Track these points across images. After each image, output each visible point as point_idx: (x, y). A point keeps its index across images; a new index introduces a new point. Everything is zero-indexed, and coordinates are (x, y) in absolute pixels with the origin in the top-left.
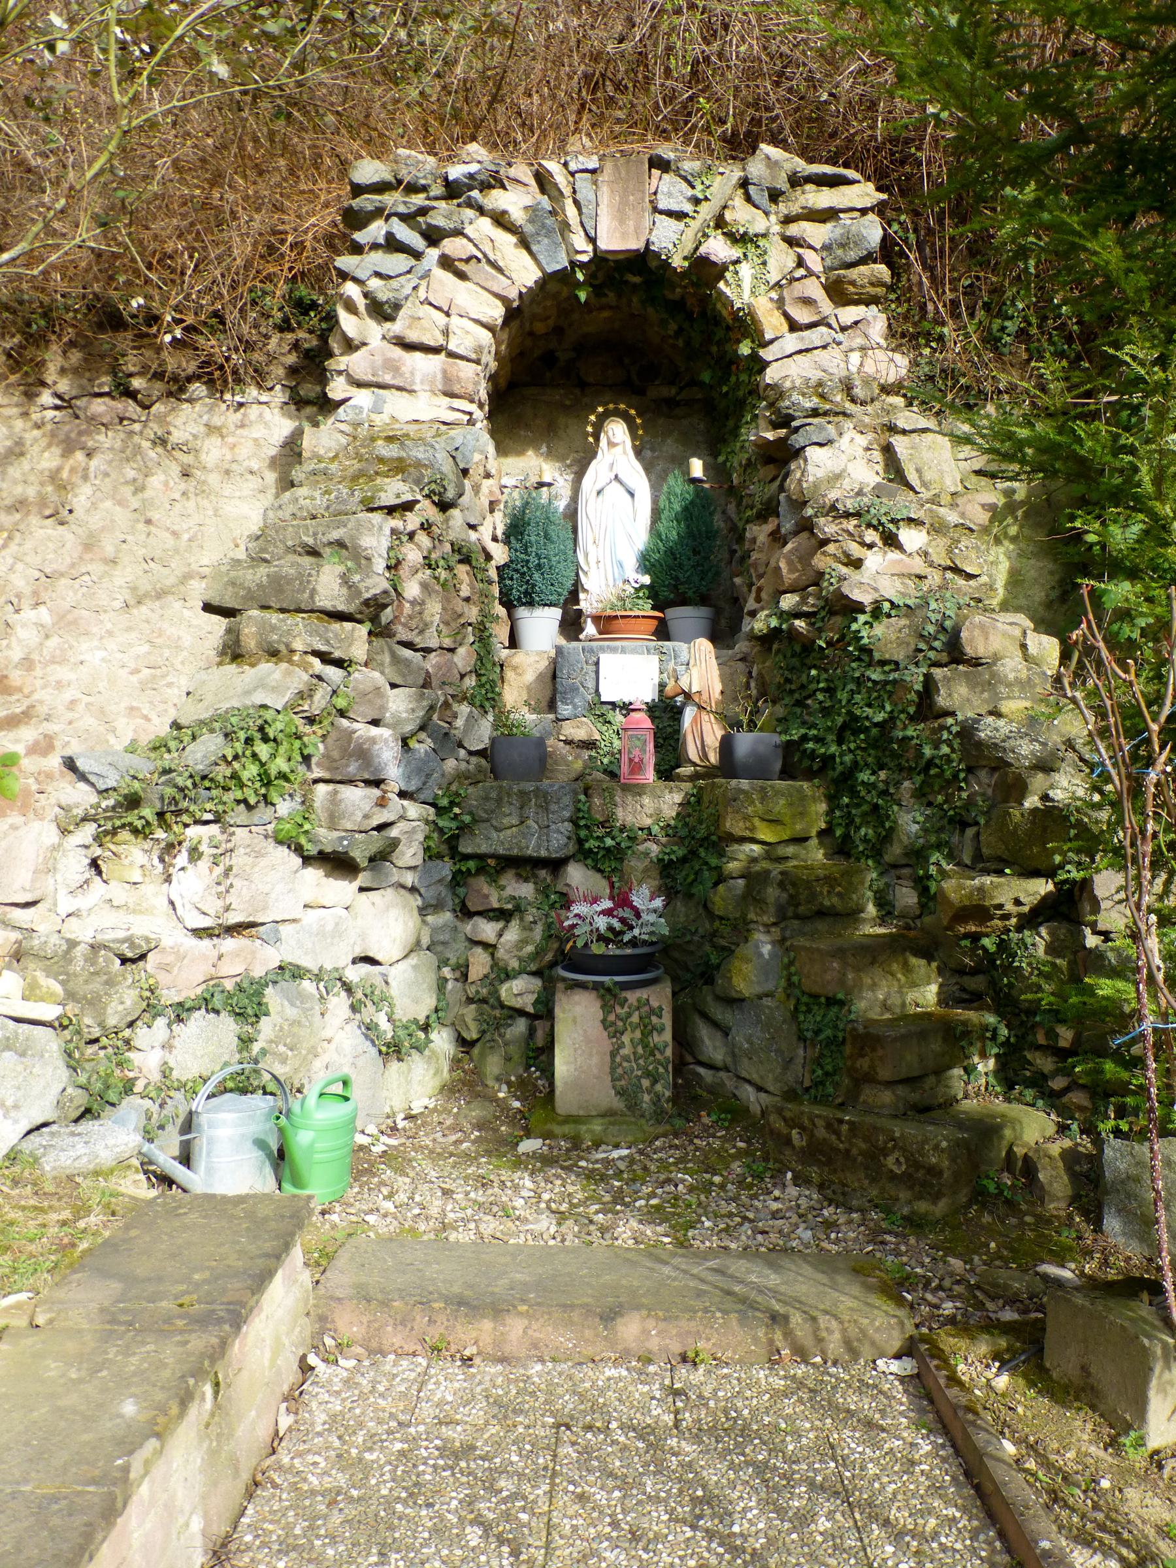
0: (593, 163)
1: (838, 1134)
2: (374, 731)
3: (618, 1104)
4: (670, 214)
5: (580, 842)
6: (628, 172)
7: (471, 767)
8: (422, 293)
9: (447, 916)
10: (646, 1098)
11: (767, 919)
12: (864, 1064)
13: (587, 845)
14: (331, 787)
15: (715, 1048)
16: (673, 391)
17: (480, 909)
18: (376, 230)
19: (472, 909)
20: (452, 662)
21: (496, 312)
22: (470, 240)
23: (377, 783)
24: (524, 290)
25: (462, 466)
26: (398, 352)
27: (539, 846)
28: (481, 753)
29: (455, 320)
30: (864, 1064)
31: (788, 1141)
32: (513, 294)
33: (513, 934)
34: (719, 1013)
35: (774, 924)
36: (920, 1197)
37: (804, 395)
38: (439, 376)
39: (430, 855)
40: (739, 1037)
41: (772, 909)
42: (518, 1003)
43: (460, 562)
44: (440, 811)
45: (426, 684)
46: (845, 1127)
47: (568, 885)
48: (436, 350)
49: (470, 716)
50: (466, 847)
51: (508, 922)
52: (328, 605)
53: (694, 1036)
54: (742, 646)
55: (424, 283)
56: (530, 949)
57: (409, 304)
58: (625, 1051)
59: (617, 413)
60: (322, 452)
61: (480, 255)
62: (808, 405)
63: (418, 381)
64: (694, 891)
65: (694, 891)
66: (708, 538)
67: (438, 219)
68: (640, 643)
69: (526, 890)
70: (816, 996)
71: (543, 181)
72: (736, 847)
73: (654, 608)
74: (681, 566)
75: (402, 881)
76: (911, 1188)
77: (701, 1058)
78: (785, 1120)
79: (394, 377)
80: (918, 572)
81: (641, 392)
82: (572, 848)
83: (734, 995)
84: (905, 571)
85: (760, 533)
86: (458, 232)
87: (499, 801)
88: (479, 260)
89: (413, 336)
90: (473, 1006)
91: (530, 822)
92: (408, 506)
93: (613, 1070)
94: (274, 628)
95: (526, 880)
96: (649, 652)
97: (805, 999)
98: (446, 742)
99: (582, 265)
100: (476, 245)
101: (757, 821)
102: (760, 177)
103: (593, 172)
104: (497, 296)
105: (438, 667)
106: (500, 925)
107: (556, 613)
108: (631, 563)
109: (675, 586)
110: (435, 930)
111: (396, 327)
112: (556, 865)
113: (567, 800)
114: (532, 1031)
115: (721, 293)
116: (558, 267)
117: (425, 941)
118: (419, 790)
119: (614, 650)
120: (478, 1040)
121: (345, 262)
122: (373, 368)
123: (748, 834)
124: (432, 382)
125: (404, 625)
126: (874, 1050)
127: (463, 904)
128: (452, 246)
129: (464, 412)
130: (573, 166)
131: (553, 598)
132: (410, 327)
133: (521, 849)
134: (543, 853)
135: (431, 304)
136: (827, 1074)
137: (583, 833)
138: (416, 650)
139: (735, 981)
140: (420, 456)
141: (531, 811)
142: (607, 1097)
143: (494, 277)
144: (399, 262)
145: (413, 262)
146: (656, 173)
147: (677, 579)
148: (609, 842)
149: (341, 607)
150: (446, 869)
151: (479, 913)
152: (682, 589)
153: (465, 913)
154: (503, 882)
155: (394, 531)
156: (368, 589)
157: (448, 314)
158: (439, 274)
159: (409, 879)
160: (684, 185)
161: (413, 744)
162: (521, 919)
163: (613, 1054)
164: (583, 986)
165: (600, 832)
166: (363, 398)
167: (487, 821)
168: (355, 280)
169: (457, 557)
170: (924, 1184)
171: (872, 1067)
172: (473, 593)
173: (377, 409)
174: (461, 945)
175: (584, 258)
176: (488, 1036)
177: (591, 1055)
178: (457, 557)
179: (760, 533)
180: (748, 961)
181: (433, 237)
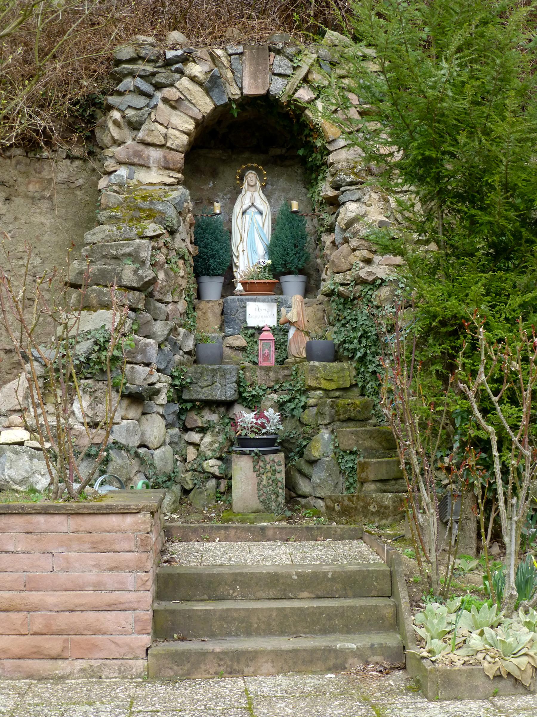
0: (240, 49)
1: (352, 501)
2: (148, 340)
3: (261, 507)
4: (280, 75)
5: (240, 393)
6: (258, 54)
7: (185, 360)
8: (153, 117)
9: (175, 431)
10: (274, 504)
11: (326, 422)
12: (363, 475)
13: (244, 395)
14: (131, 365)
15: (305, 486)
16: (284, 151)
17: (193, 426)
18: (128, 83)
19: (189, 426)
20: (176, 307)
21: (190, 126)
22: (178, 89)
23: (148, 365)
24: (205, 115)
25: (179, 210)
26: (141, 147)
27: (221, 395)
28: (189, 353)
29: (171, 131)
30: (363, 475)
31: (334, 509)
32: (199, 117)
33: (208, 439)
34: (305, 468)
35: (329, 424)
36: (382, 519)
37: (346, 175)
38: (162, 160)
39: (171, 401)
40: (316, 479)
41: (328, 417)
42: (212, 470)
43: (180, 258)
44: (173, 377)
45: (167, 319)
46: (355, 498)
47: (235, 414)
48: (161, 146)
49: (185, 334)
50: (186, 396)
51: (205, 434)
52: (128, 283)
53: (295, 483)
54: (320, 297)
55: (154, 111)
56: (217, 445)
57: (147, 123)
58: (263, 483)
59: (252, 168)
60: (111, 205)
61: (183, 97)
62: (349, 180)
63: (151, 162)
64: (294, 413)
65: (294, 413)
66: (302, 238)
67: (160, 79)
68: (267, 297)
69: (214, 418)
70: (345, 451)
71: (214, 58)
72: (313, 392)
73: (274, 278)
74: (288, 254)
75: (158, 411)
76: (379, 516)
77: (300, 493)
78: (332, 501)
79: (139, 160)
80: (398, 263)
81: (265, 152)
82: (236, 396)
83: (313, 458)
84: (392, 263)
85: (327, 239)
86: (172, 85)
87: (202, 374)
88: (183, 100)
89: (149, 139)
90: (190, 473)
91: (217, 384)
92: (158, 236)
93: (258, 491)
94: (105, 294)
95: (214, 413)
96: (272, 301)
97: (342, 453)
98: (176, 347)
99: (235, 101)
100: (180, 92)
101: (322, 380)
102: (326, 56)
103: (241, 54)
104: (191, 117)
105: (172, 310)
106: (202, 435)
107: (221, 279)
108: (261, 249)
109: (285, 265)
110: (172, 436)
111: (141, 135)
112: (228, 405)
113: (234, 373)
114: (218, 486)
115: (306, 115)
116: (223, 102)
117: (168, 441)
118: (165, 369)
119: (255, 301)
120: (192, 489)
121: (112, 100)
122: (128, 155)
123: (318, 386)
124: (159, 163)
125: (158, 291)
126: (367, 468)
127: (184, 425)
128: (170, 93)
129: (175, 178)
130: (231, 51)
131: (220, 272)
132: (147, 135)
133: (213, 396)
134: (223, 398)
135: (157, 122)
136: (351, 484)
137: (241, 389)
138: (163, 303)
139: (313, 452)
140: (161, 208)
141: (218, 378)
142: (255, 504)
143: (190, 108)
144: (141, 101)
145: (147, 101)
146: (273, 54)
147: (286, 261)
148: (254, 393)
149: (135, 285)
150: (176, 407)
151: (192, 429)
152: (289, 266)
153: (185, 429)
154: (203, 414)
155: (153, 248)
156: (146, 276)
157: (167, 128)
158: (161, 105)
159: (161, 410)
160: (287, 61)
161: (163, 347)
162: (213, 431)
163: (259, 485)
164: (243, 453)
165: (250, 389)
166: (123, 172)
167: (196, 383)
168: (118, 110)
169: (178, 257)
170: (383, 514)
171: (367, 476)
172: (185, 273)
173: (130, 177)
174: (183, 445)
175: (236, 97)
176: (197, 486)
177: (248, 485)
178: (178, 257)
179: (327, 239)
180: (318, 442)
181: (158, 87)
